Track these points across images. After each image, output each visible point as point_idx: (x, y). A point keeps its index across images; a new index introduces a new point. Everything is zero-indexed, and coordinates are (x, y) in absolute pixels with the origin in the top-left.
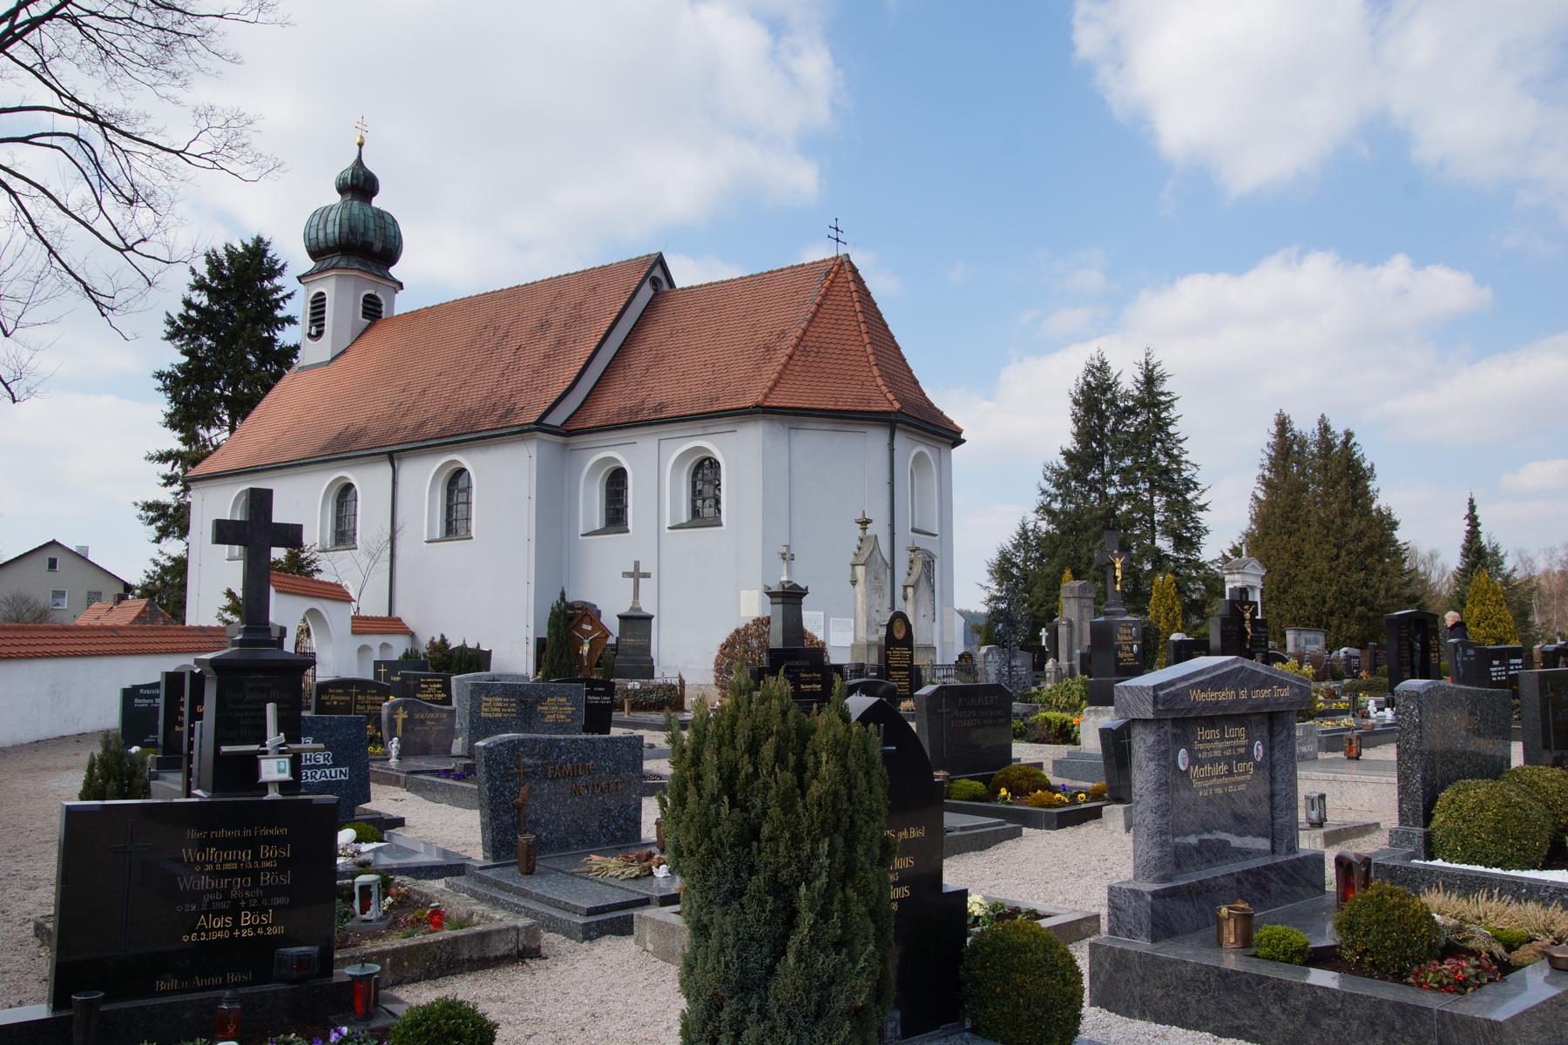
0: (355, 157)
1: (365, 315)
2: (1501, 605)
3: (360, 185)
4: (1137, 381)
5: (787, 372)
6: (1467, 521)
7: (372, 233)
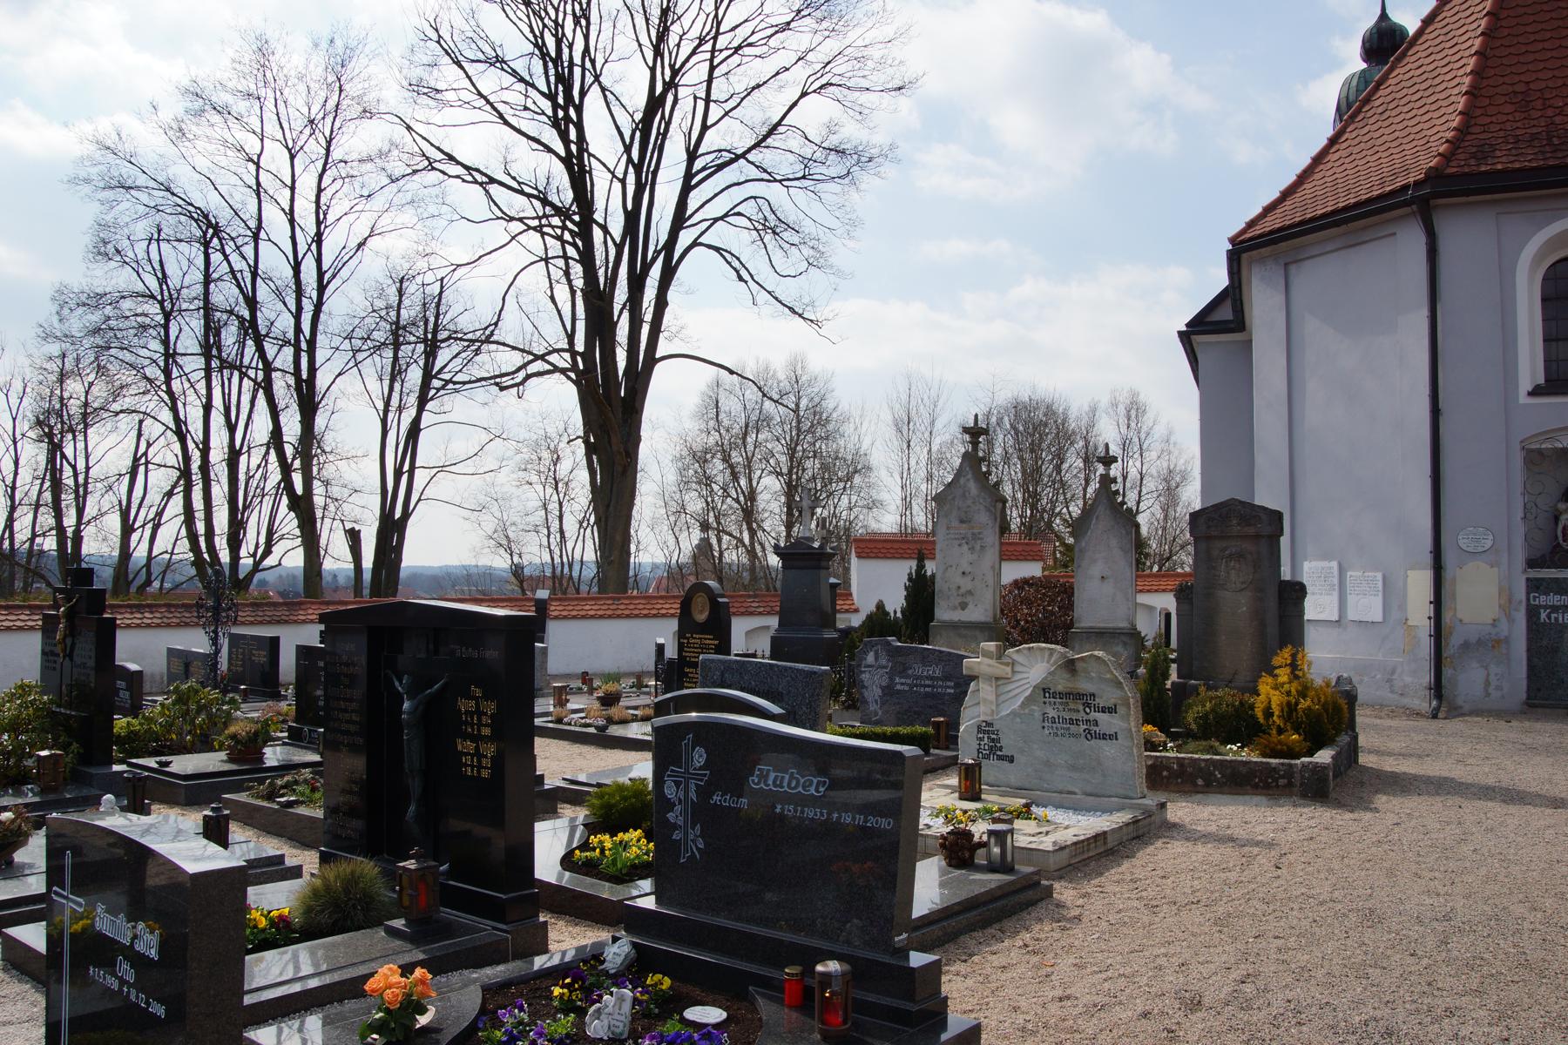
0: (1378, 12)
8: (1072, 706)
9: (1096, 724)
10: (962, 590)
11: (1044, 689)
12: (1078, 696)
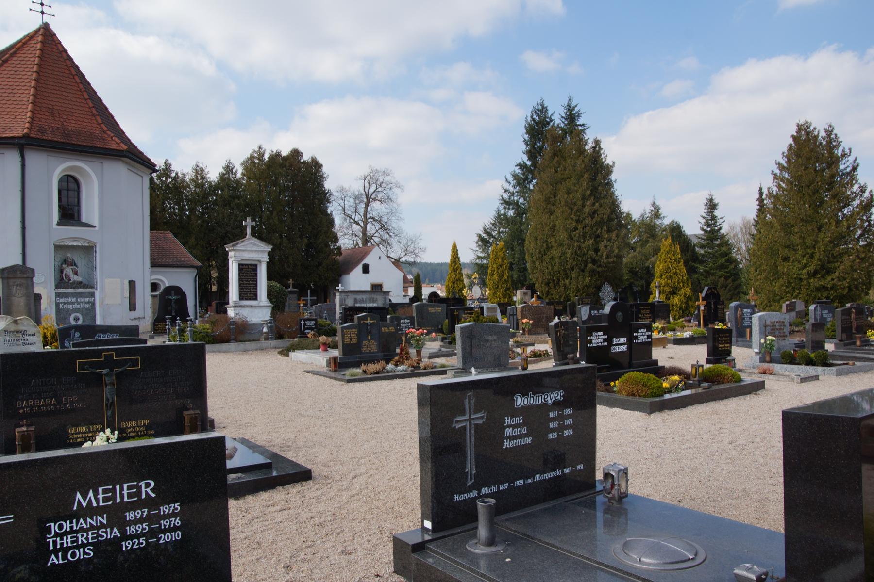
2: (679, 262)
4: (562, 117)
5: (34, 122)
6: (758, 203)
8: (17, 335)
9: (27, 340)
11: (5, 331)
12: (20, 332)
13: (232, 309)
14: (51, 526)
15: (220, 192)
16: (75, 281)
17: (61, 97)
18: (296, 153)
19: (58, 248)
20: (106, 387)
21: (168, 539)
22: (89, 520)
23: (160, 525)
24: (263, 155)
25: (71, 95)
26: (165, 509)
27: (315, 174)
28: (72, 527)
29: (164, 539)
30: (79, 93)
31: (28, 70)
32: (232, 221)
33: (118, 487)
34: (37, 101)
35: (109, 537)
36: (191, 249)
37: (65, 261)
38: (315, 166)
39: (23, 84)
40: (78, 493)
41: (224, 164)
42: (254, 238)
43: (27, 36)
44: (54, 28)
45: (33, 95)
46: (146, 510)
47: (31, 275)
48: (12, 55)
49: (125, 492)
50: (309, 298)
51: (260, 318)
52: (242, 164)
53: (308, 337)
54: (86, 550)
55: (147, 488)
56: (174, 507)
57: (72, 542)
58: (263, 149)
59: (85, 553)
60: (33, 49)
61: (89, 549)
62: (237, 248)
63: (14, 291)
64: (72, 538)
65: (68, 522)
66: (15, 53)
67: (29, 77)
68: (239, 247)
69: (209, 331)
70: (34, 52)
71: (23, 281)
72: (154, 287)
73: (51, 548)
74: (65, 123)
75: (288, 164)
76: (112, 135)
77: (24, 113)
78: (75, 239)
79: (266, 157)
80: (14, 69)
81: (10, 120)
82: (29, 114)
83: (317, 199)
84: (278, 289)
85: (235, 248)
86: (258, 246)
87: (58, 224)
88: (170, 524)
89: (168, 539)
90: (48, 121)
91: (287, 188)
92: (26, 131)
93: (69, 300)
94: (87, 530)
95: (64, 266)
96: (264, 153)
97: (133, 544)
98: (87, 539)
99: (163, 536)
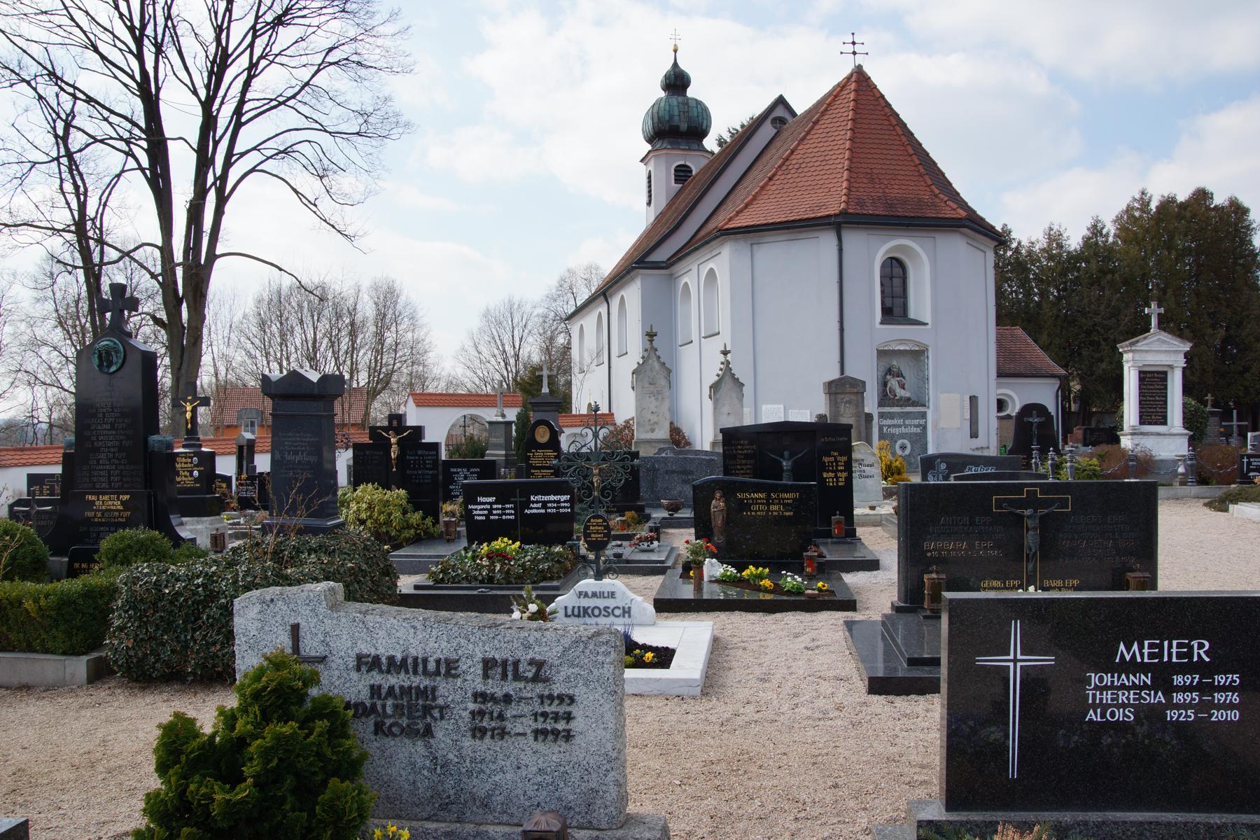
0: (673, 62)
1: (677, 181)
3: (676, 82)
7: (676, 118)
9: (864, 471)
10: (652, 422)
13: (1129, 437)
14: (1091, 676)
15: (1083, 265)
16: (901, 397)
17: (880, 156)
18: (1202, 196)
19: (882, 354)
20: (1027, 532)
21: (1222, 717)
22: (1131, 677)
23: (1214, 697)
24: (1148, 203)
25: (892, 152)
26: (1220, 679)
27: (1236, 224)
28: (1112, 682)
29: (1217, 717)
30: (902, 148)
31: (841, 128)
32: (1102, 308)
33: (1166, 643)
34: (853, 165)
35: (1152, 701)
36: (1045, 348)
37: (889, 371)
38: (1237, 211)
39: (836, 147)
40: (1122, 644)
41: (1089, 222)
42: (1163, 333)
43: (838, 84)
44: (868, 69)
45: (848, 159)
46: (1198, 676)
47: (860, 389)
48: (823, 114)
49: (1174, 650)
50: (1235, 423)
51: (1172, 451)
52: (1115, 221)
53: (1254, 483)
54: (1127, 712)
55: (1201, 650)
56: (1232, 678)
57: (1112, 699)
58: (1148, 195)
59: (1125, 715)
60: (845, 101)
61: (1129, 711)
62: (1137, 348)
63: (842, 410)
64: (1112, 694)
65: (1109, 675)
66: (826, 110)
67: (843, 137)
68: (1140, 346)
69: (1097, 468)
70: (847, 105)
71: (853, 397)
72: (1001, 405)
73: (1090, 702)
74: (887, 190)
75: (1188, 215)
76: (946, 198)
77: (839, 184)
78: (902, 341)
79: (1153, 206)
80: (826, 131)
81: (824, 194)
82: (845, 184)
83: (1240, 265)
84: (1193, 409)
85: (1133, 348)
86: (1169, 344)
87: (882, 323)
88: (1226, 700)
89: (1222, 717)
90: (867, 190)
91: (1187, 251)
92: (843, 206)
93: (895, 422)
94: (1128, 689)
95: (888, 377)
96: (1150, 200)
97: (1180, 715)
98: (1128, 698)
99: (1216, 712)
